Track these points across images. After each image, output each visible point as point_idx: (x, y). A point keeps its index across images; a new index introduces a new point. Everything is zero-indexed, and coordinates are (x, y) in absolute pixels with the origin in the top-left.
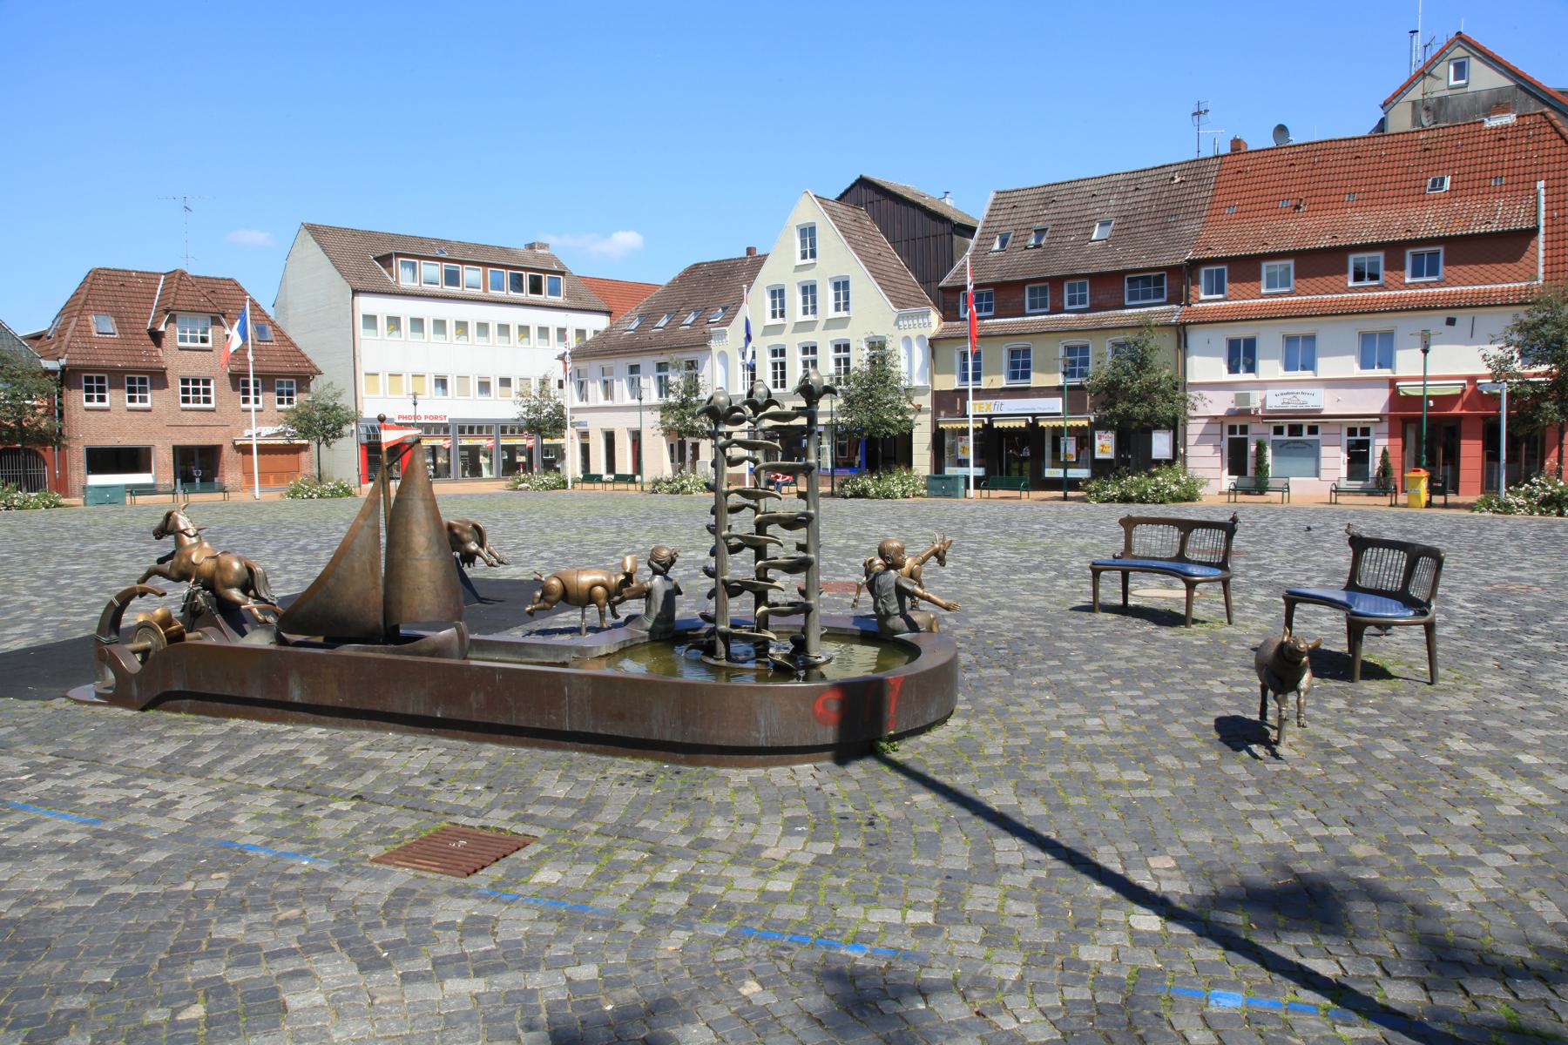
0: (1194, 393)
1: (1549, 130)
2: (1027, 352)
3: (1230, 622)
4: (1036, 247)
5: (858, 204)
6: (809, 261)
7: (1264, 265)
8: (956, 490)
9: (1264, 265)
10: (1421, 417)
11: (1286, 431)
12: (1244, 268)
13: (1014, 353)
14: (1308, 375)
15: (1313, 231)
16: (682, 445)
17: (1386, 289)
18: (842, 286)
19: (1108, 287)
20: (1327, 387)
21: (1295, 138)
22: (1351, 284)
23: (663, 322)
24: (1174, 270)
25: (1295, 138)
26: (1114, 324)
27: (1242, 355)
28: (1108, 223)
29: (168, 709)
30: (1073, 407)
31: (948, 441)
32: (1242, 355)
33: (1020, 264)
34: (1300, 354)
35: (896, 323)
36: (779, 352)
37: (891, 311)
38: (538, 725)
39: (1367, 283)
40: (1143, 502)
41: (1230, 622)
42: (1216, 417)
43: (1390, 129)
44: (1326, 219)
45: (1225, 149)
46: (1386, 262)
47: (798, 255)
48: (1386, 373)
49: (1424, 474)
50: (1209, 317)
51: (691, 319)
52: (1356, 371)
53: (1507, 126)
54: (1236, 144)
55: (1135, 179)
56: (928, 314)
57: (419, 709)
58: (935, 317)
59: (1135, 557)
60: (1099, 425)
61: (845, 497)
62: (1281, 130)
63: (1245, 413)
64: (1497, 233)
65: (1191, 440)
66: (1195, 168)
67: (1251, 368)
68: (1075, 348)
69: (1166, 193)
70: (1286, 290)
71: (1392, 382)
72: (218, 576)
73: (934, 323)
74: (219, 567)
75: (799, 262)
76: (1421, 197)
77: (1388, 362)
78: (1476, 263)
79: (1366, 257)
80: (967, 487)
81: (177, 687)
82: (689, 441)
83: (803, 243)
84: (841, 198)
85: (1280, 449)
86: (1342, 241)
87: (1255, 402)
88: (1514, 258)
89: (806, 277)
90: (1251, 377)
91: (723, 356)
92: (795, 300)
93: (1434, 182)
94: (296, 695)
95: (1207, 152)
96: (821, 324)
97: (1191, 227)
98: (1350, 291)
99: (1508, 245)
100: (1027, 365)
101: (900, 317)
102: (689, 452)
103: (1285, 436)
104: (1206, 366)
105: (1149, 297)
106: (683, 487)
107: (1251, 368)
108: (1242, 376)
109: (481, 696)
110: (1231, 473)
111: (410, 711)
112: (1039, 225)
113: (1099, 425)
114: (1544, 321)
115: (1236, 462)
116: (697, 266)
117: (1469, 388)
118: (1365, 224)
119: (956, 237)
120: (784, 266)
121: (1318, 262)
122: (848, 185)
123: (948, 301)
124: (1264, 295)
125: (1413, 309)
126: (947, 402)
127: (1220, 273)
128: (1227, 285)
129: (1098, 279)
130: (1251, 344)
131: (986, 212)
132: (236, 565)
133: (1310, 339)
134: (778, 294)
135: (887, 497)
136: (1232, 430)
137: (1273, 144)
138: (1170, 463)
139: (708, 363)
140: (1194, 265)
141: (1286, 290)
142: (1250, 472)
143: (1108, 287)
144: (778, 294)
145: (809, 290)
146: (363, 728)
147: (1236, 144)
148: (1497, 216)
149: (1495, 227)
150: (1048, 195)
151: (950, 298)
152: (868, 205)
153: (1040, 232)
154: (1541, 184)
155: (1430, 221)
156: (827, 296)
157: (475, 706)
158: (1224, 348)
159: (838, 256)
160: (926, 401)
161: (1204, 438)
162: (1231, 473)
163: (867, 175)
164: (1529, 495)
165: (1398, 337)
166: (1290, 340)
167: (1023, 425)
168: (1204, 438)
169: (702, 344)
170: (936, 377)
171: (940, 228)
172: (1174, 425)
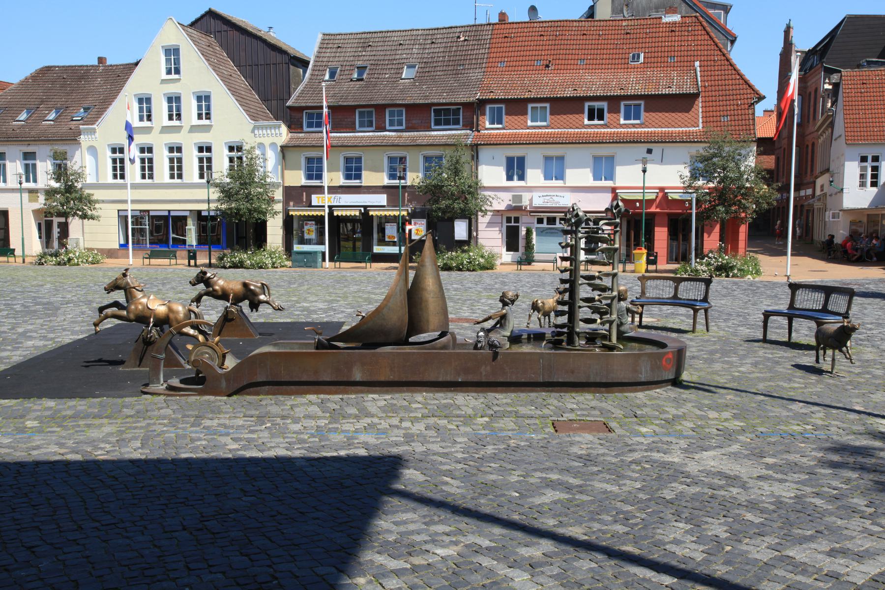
0: (487, 193)
1: (700, 28)
2: (359, 160)
3: (708, 330)
4: (358, 80)
5: (207, 32)
6: (173, 76)
7: (530, 106)
8: (316, 262)
9: (530, 106)
10: (642, 213)
11: (545, 221)
12: (517, 106)
13: (348, 160)
14: (559, 183)
15: (561, 84)
16: (49, 225)
17: (608, 127)
18: (204, 99)
19: (419, 114)
20: (573, 191)
21: (543, 16)
22: (586, 122)
23: (23, 116)
24: (467, 106)
25: (543, 16)
26: (425, 142)
27: (516, 168)
28: (414, 67)
29: (248, 394)
30: (393, 202)
31: (295, 226)
32: (516, 168)
33: (351, 92)
34: (555, 168)
35: (253, 131)
36: (176, 149)
37: (248, 123)
38: (523, 380)
39: (596, 122)
40: (460, 270)
41: (708, 330)
42: (498, 211)
43: (598, 17)
44: (568, 76)
45: (495, 19)
46: (609, 109)
47: (164, 71)
48: (609, 184)
49: (645, 251)
50: (493, 141)
51: (52, 116)
52: (590, 182)
53: (675, 23)
54: (503, 16)
55: (431, 35)
56: (279, 127)
57: (449, 378)
58: (284, 129)
59: (648, 298)
60: (414, 215)
61: (224, 267)
62: (533, 9)
63: (519, 209)
64: (676, 94)
65: (481, 227)
66: (475, 30)
67: (522, 177)
68: (396, 158)
69: (458, 47)
70: (544, 124)
71: (613, 190)
72: (171, 316)
73: (282, 134)
74: (170, 310)
75: (165, 76)
76: (626, 67)
77: (610, 176)
78: (667, 112)
79: (597, 104)
80: (324, 260)
81: (260, 378)
82: (56, 220)
83: (168, 61)
84: (192, 25)
85: (541, 232)
86: (581, 94)
87: (525, 202)
88: (688, 110)
89: (172, 89)
90: (522, 183)
91: (93, 150)
92: (160, 109)
93: (634, 56)
94: (358, 376)
95: (482, 20)
96: (186, 128)
97: (475, 75)
98: (587, 126)
99: (681, 102)
100: (359, 169)
101: (255, 128)
102: (56, 231)
103: (545, 225)
104: (491, 174)
105: (441, 125)
106: (70, 260)
107: (522, 177)
108: (516, 183)
109: (488, 368)
110: (508, 250)
111: (440, 379)
112: (360, 63)
113: (414, 215)
114: (714, 155)
115: (512, 244)
116: (48, 69)
117: (660, 195)
118: (593, 82)
119: (291, 67)
120: (149, 78)
121: (565, 106)
122: (198, 15)
123: (294, 118)
124: (533, 125)
125: (627, 142)
126: (292, 194)
127: (500, 109)
128: (504, 117)
129: (412, 108)
130: (521, 161)
131: (316, 49)
132: (180, 308)
133: (561, 159)
134: (145, 101)
135: (261, 268)
136: (509, 220)
137: (527, 20)
138: (467, 243)
139: (78, 153)
140: (482, 103)
141: (544, 124)
142: (521, 249)
143: (419, 114)
144: (145, 101)
145: (174, 100)
146: (404, 392)
147: (503, 16)
148: (674, 83)
149: (674, 90)
150: (366, 41)
151: (296, 115)
152: (217, 33)
153: (362, 69)
154: (697, 64)
155: (634, 83)
156: (190, 108)
157: (484, 373)
158: (504, 161)
159: (199, 73)
160: (278, 195)
161: (490, 224)
162: (508, 250)
163: (214, 8)
164: (709, 264)
165: (617, 159)
166: (548, 159)
167: (357, 213)
168: (490, 224)
169: (73, 138)
170: (286, 172)
171: (279, 57)
172: (470, 216)
